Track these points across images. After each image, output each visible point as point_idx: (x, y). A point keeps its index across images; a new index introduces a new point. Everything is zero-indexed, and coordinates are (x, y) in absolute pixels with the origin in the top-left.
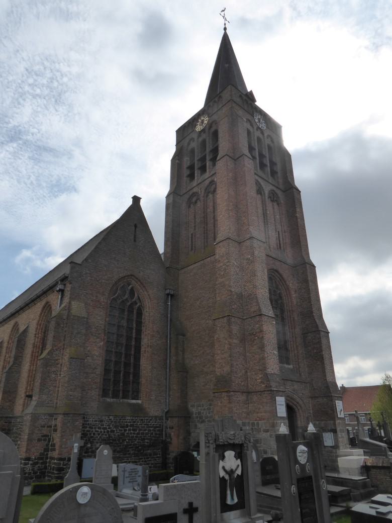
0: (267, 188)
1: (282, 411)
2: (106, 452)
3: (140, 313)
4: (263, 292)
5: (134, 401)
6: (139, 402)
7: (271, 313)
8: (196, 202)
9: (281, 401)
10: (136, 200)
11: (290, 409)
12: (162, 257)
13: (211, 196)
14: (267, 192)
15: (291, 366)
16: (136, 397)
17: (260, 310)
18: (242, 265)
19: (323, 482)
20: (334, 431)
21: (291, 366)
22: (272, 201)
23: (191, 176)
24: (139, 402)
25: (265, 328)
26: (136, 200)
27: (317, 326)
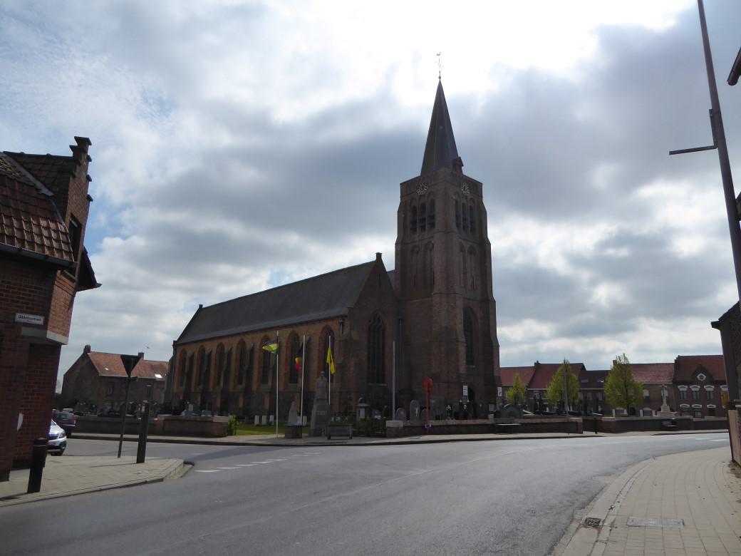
0: (467, 246)
1: (465, 392)
2: (402, 413)
3: (384, 331)
4: (460, 327)
5: (382, 385)
6: (385, 385)
7: (464, 340)
8: (418, 252)
9: (465, 388)
10: (379, 255)
11: (470, 390)
12: (392, 278)
13: (428, 252)
14: (467, 249)
15: (474, 367)
16: (383, 382)
17: (457, 338)
18: (449, 315)
19: (20, 317)
20: (495, 404)
21: (474, 367)
22: (471, 254)
23: (414, 230)
24: (385, 385)
25: (460, 349)
26: (379, 255)
27: (492, 343)
